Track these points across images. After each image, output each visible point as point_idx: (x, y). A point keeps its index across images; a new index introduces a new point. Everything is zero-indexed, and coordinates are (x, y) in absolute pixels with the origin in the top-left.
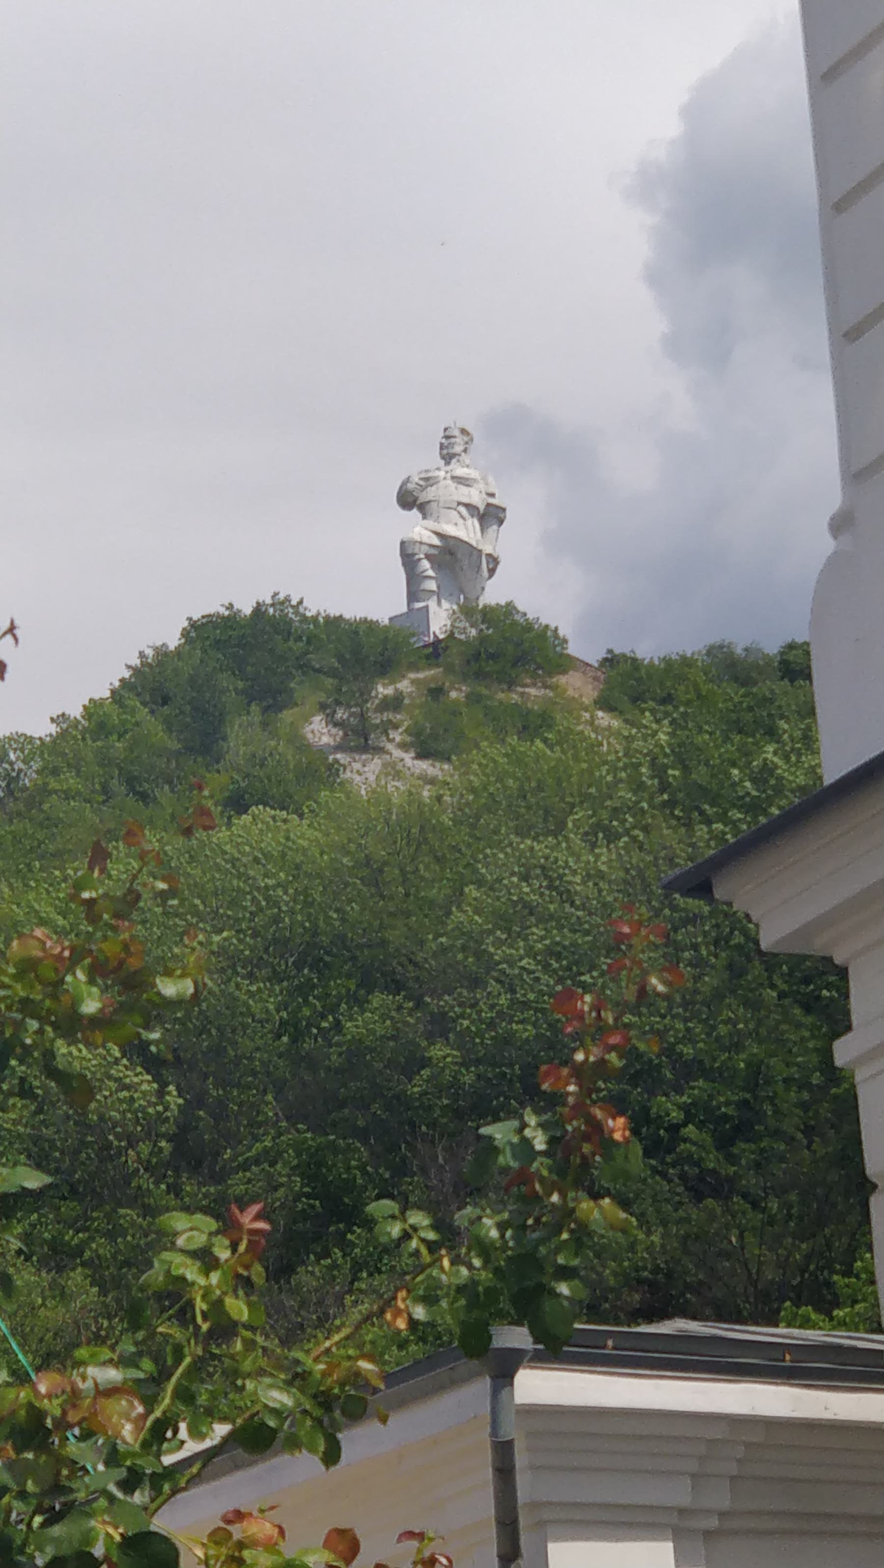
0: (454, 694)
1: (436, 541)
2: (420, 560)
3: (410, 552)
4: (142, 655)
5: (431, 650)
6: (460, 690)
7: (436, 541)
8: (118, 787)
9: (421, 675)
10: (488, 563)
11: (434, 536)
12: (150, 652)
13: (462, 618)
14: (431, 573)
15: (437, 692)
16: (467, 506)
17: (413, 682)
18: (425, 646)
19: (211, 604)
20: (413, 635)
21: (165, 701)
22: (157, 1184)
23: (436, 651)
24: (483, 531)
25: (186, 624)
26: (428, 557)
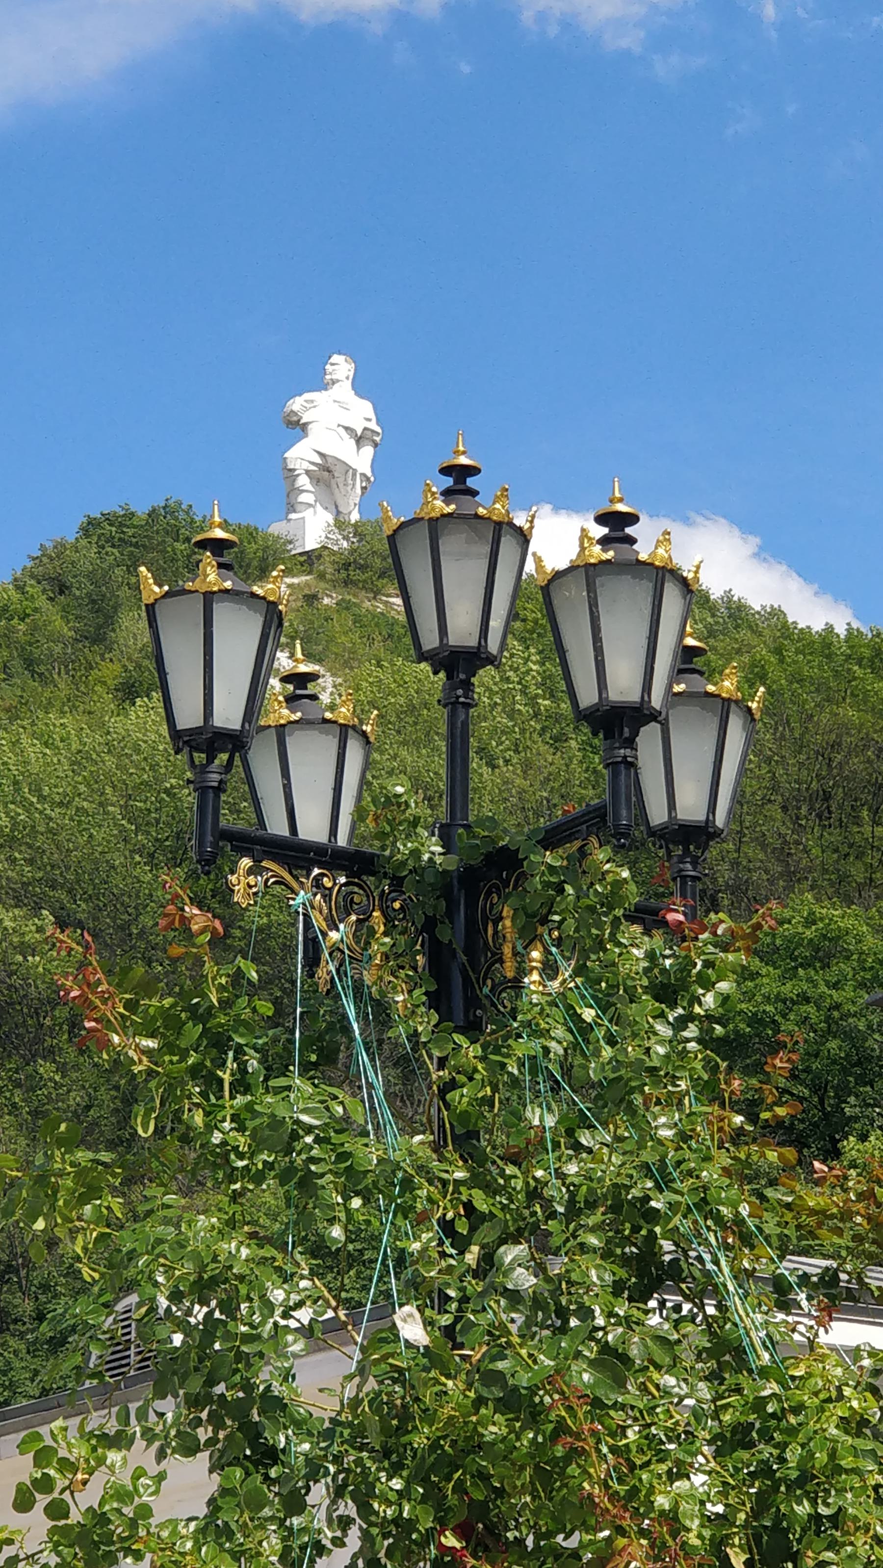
0: (326, 601)
1: (318, 460)
2: (298, 475)
3: (291, 466)
4: (42, 547)
5: (305, 558)
6: (331, 597)
7: (318, 460)
8: (17, 664)
9: (296, 580)
10: (362, 481)
11: (316, 455)
12: (49, 545)
13: (336, 531)
14: (309, 487)
15: (311, 599)
16: (347, 429)
17: (289, 586)
18: (301, 554)
19: (109, 503)
20: (290, 542)
21: (63, 589)
22: (385, 934)
23: (310, 559)
24: (359, 448)
25: (85, 520)
26: (307, 472)
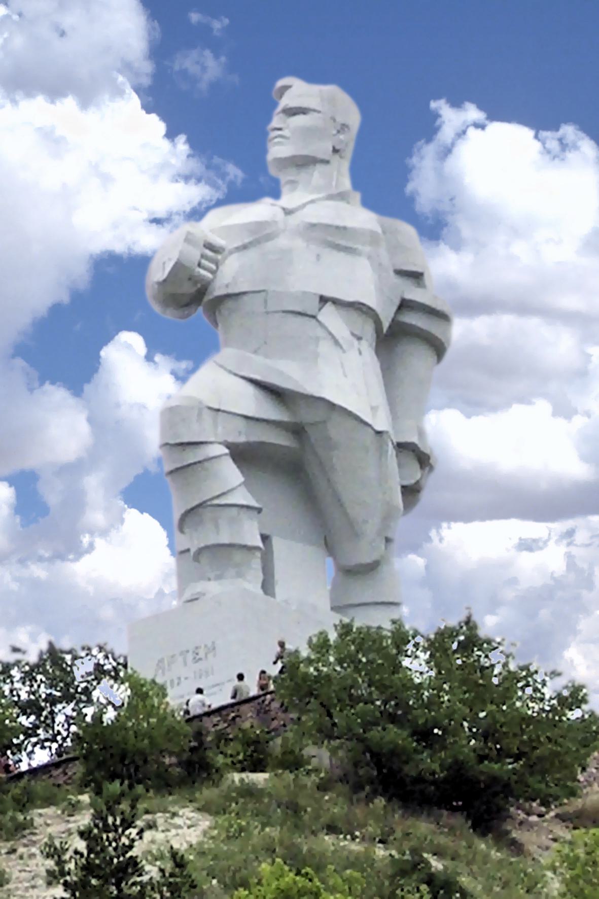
1: (270, 411)
